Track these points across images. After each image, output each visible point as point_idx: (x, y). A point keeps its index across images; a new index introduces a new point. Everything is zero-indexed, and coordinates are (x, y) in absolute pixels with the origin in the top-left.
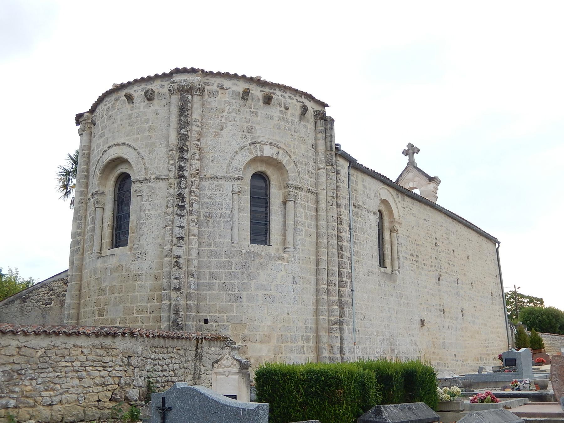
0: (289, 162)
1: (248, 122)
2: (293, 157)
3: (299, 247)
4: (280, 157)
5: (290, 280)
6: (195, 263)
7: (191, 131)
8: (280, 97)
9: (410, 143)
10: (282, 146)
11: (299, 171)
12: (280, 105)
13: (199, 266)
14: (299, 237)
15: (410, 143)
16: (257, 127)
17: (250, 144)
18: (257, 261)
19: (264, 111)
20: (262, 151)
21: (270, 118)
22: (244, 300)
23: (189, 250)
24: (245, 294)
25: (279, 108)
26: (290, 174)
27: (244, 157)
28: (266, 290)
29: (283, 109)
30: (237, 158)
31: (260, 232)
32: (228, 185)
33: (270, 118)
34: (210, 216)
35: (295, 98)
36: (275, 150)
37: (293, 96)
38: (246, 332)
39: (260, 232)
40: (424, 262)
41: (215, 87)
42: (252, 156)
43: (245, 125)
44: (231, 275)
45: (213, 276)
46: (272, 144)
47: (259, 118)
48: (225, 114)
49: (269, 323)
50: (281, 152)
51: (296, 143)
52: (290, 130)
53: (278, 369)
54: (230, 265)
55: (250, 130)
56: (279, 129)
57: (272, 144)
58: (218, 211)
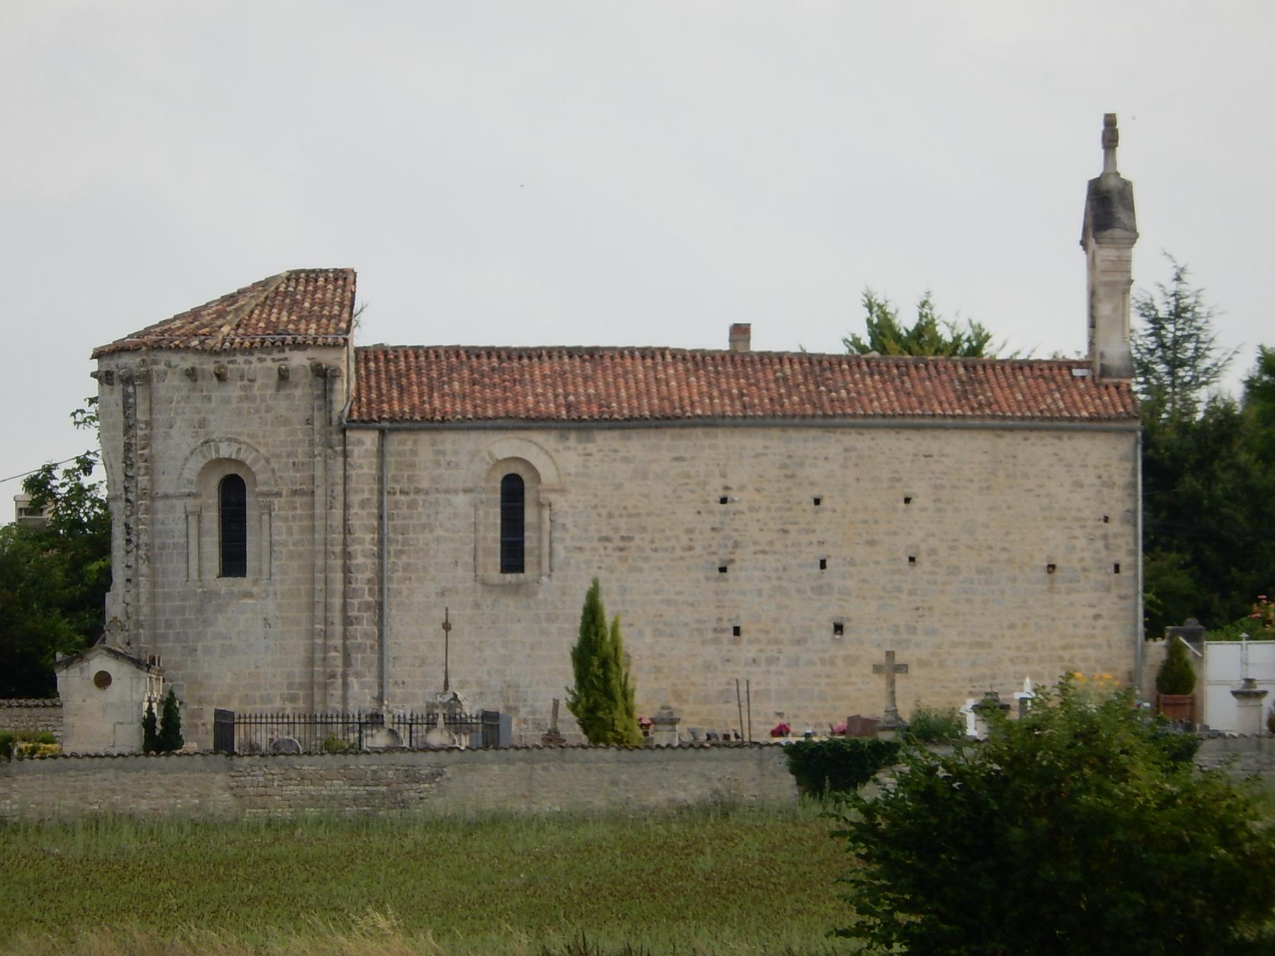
0: (256, 460)
1: (199, 413)
2: (263, 450)
3: (277, 577)
4: (242, 456)
5: (261, 622)
6: (145, 610)
7: (135, 436)
8: (243, 365)
9: (1114, 115)
10: (242, 439)
11: (273, 470)
12: (242, 378)
13: (154, 611)
14: (275, 563)
15: (1114, 115)
16: (211, 417)
17: (203, 444)
18: (214, 602)
19: (218, 393)
20: (217, 451)
21: (226, 400)
22: (199, 652)
23: (138, 594)
24: (200, 645)
25: (239, 383)
26: (260, 477)
27: (197, 463)
28: (224, 638)
29: (246, 382)
30: (188, 466)
31: (233, 560)
32: (179, 505)
33: (226, 400)
34: (163, 547)
35: (269, 358)
36: (235, 446)
37: (263, 356)
38: (202, 693)
39: (233, 560)
40: (587, 555)
41: (162, 367)
42: (205, 461)
43: (197, 417)
44: (185, 623)
45: (169, 625)
46: (230, 440)
47: (213, 404)
48: (173, 405)
49: (229, 681)
50: (244, 447)
51: (269, 428)
52: (257, 411)
53: (1057, 731)
54: (184, 608)
55: (203, 423)
56: (239, 414)
57: (230, 440)
58: (170, 541)
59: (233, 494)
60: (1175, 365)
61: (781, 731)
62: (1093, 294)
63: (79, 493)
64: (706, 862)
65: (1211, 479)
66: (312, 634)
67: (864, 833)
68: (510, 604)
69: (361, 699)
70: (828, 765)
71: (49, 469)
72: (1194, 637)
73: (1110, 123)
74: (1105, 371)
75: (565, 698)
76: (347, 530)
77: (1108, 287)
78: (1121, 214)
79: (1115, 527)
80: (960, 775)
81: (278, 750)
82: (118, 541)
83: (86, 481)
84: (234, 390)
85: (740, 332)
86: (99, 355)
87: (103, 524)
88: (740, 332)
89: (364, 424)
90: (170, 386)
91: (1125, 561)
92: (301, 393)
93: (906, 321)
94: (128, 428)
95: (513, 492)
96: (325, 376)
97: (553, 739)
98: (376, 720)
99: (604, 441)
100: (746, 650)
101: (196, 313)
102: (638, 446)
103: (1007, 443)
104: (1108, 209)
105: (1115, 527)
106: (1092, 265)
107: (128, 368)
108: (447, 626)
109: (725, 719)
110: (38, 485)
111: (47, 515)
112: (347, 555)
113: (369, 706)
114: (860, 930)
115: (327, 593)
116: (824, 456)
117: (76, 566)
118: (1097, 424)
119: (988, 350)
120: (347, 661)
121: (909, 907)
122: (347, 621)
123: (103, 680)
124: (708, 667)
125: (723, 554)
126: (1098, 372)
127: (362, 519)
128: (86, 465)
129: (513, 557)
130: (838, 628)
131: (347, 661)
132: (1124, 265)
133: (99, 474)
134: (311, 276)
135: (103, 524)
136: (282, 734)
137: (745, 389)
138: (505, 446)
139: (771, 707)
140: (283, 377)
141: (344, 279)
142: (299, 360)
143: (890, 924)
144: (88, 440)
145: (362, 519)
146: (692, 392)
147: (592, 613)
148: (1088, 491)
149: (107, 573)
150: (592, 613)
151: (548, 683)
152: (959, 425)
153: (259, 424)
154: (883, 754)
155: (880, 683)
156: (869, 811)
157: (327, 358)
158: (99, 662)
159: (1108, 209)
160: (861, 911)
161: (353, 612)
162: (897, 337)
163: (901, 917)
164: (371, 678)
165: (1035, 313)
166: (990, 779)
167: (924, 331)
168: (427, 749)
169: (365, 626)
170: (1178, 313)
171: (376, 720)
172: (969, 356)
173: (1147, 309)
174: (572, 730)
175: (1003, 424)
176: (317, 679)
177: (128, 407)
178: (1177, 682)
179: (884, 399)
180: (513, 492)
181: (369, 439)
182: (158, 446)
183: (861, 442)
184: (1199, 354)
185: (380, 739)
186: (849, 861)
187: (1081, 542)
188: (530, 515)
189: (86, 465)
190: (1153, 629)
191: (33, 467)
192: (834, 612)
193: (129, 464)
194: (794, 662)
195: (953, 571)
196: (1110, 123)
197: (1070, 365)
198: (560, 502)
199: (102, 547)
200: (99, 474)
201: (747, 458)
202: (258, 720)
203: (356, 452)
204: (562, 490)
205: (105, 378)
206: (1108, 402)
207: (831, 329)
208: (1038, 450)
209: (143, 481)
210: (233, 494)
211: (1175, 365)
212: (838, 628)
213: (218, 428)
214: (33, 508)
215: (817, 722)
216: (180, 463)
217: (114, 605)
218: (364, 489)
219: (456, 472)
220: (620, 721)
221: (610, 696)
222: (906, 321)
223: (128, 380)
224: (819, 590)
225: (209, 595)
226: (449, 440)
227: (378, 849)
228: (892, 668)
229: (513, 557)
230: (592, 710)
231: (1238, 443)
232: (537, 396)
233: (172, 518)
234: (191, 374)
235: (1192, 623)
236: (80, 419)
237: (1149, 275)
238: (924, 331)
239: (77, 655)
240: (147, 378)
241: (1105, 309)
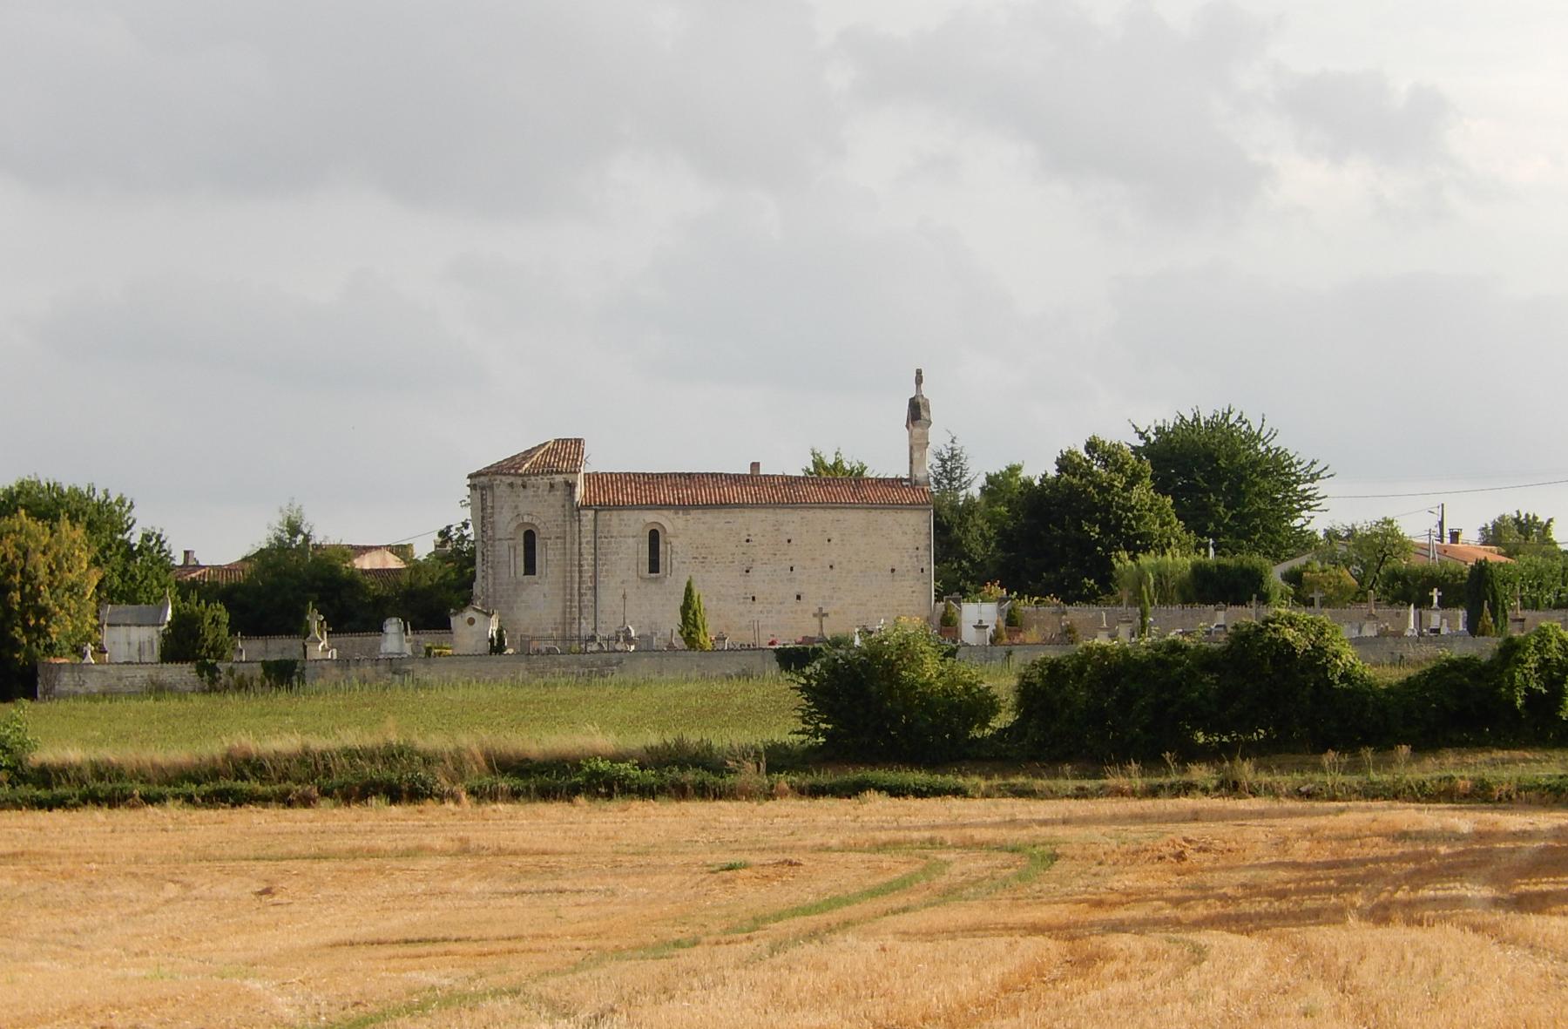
19: (522, 493)
27: (514, 525)
31: (530, 568)
39: (530, 568)
59: (530, 538)
60: (951, 480)
61: (772, 643)
62: (911, 448)
63: (463, 538)
64: (739, 701)
65: (966, 531)
66: (565, 601)
67: (804, 688)
68: (653, 586)
69: (587, 629)
70: (791, 659)
71: (449, 527)
72: (957, 601)
73: (919, 373)
74: (917, 483)
75: (676, 629)
76: (580, 554)
77: (917, 447)
78: (923, 413)
79: (921, 552)
80: (848, 662)
81: (549, 651)
82: (479, 555)
83: (466, 532)
84: (530, 492)
85: (755, 466)
86: (470, 477)
87: (473, 551)
88: (755, 466)
89: (588, 507)
90: (501, 490)
91: (926, 568)
92: (560, 493)
93: (830, 461)
94: (483, 509)
95: (654, 537)
96: (571, 487)
97: (671, 646)
98: (593, 639)
99: (695, 514)
100: (758, 606)
101: (513, 458)
102: (710, 517)
103: (875, 514)
104: (917, 412)
105: (921, 552)
106: (911, 436)
107: (483, 483)
108: (624, 596)
109: (748, 638)
110: (444, 534)
111: (448, 548)
112: (580, 566)
113: (590, 632)
114: (803, 732)
115: (572, 581)
116: (792, 520)
117: (461, 571)
118: (913, 506)
119: (867, 474)
120: (580, 613)
121: (824, 721)
122: (580, 595)
123: (471, 621)
124: (741, 615)
125: (748, 564)
126: (912, 483)
127: (587, 550)
128: (466, 525)
129: (654, 566)
130: (799, 597)
131: (580, 613)
132: (925, 436)
133: (471, 529)
134: (565, 441)
135: (473, 551)
136: (551, 644)
137: (754, 490)
138: (651, 517)
139: (770, 632)
140: (552, 486)
141: (578, 441)
142: (559, 478)
143: (817, 729)
144: (467, 514)
145: (587, 550)
146: (733, 493)
147: (689, 591)
148: (911, 533)
149: (474, 574)
150: (689, 591)
151: (670, 622)
152: (852, 507)
153: (542, 510)
154: (817, 653)
155: (816, 621)
156: (808, 678)
157: (570, 478)
158: (469, 613)
159: (917, 412)
160: (805, 722)
161: (582, 591)
162: (825, 468)
163: (823, 726)
164: (591, 620)
165: (886, 457)
166: (861, 664)
167: (837, 466)
168: (615, 651)
169: (588, 597)
170: (952, 457)
171: (593, 639)
172: (857, 479)
173: (939, 455)
174: (679, 643)
175: (871, 506)
176: (567, 622)
177: (483, 500)
178: (948, 624)
179: (819, 495)
180: (654, 537)
181: (591, 513)
182: (496, 517)
183: (809, 514)
184: (961, 476)
185: (595, 647)
186: (801, 700)
187: (906, 559)
188: (662, 548)
189: (466, 525)
190: (939, 599)
191: (443, 527)
192: (796, 590)
193: (483, 525)
194: (779, 612)
195: (850, 572)
196: (919, 373)
197: (901, 480)
198: (675, 542)
199: (472, 562)
200: (471, 529)
201: (757, 522)
202: (540, 639)
203: (584, 519)
204: (676, 537)
205: (473, 487)
206: (918, 497)
207: (795, 464)
208: (888, 518)
209: (490, 533)
210: (530, 538)
211: (951, 480)
212: (799, 597)
213: (523, 509)
214: (443, 544)
215: (789, 638)
216: (507, 524)
217: (477, 588)
218: (588, 537)
219: (630, 528)
220: (702, 638)
221: (696, 627)
222: (830, 461)
223: (483, 488)
224: (790, 580)
225: (519, 583)
226: (625, 514)
227: (1250, 785)
228: (821, 615)
229: (654, 566)
230: (689, 634)
231: (977, 515)
232: (665, 494)
233: (503, 548)
234: (511, 485)
235: (956, 595)
236: (463, 504)
237: (938, 439)
238: (837, 466)
239: (460, 610)
240: (491, 487)
241: (916, 455)
